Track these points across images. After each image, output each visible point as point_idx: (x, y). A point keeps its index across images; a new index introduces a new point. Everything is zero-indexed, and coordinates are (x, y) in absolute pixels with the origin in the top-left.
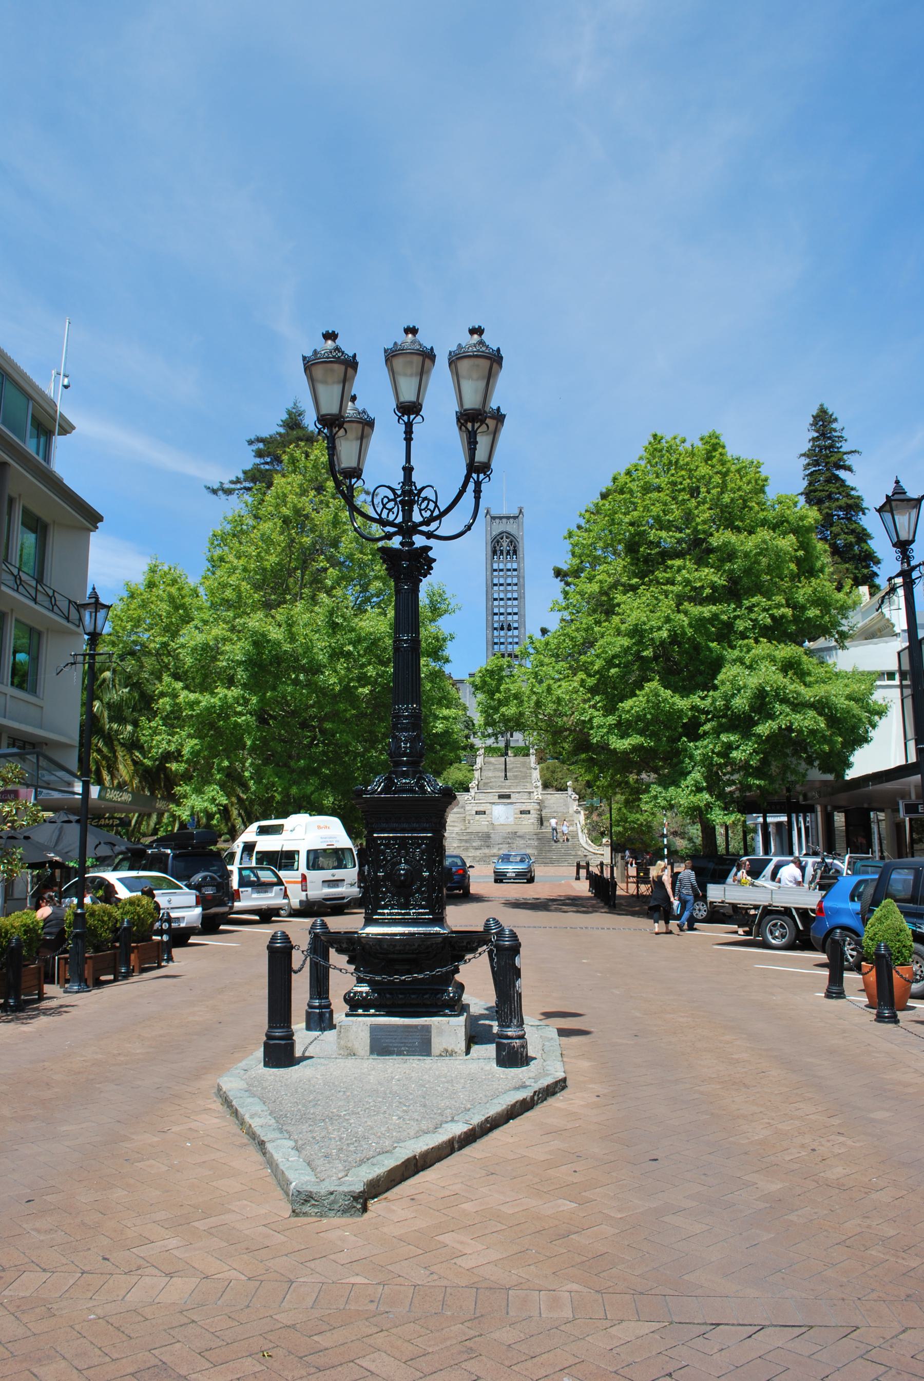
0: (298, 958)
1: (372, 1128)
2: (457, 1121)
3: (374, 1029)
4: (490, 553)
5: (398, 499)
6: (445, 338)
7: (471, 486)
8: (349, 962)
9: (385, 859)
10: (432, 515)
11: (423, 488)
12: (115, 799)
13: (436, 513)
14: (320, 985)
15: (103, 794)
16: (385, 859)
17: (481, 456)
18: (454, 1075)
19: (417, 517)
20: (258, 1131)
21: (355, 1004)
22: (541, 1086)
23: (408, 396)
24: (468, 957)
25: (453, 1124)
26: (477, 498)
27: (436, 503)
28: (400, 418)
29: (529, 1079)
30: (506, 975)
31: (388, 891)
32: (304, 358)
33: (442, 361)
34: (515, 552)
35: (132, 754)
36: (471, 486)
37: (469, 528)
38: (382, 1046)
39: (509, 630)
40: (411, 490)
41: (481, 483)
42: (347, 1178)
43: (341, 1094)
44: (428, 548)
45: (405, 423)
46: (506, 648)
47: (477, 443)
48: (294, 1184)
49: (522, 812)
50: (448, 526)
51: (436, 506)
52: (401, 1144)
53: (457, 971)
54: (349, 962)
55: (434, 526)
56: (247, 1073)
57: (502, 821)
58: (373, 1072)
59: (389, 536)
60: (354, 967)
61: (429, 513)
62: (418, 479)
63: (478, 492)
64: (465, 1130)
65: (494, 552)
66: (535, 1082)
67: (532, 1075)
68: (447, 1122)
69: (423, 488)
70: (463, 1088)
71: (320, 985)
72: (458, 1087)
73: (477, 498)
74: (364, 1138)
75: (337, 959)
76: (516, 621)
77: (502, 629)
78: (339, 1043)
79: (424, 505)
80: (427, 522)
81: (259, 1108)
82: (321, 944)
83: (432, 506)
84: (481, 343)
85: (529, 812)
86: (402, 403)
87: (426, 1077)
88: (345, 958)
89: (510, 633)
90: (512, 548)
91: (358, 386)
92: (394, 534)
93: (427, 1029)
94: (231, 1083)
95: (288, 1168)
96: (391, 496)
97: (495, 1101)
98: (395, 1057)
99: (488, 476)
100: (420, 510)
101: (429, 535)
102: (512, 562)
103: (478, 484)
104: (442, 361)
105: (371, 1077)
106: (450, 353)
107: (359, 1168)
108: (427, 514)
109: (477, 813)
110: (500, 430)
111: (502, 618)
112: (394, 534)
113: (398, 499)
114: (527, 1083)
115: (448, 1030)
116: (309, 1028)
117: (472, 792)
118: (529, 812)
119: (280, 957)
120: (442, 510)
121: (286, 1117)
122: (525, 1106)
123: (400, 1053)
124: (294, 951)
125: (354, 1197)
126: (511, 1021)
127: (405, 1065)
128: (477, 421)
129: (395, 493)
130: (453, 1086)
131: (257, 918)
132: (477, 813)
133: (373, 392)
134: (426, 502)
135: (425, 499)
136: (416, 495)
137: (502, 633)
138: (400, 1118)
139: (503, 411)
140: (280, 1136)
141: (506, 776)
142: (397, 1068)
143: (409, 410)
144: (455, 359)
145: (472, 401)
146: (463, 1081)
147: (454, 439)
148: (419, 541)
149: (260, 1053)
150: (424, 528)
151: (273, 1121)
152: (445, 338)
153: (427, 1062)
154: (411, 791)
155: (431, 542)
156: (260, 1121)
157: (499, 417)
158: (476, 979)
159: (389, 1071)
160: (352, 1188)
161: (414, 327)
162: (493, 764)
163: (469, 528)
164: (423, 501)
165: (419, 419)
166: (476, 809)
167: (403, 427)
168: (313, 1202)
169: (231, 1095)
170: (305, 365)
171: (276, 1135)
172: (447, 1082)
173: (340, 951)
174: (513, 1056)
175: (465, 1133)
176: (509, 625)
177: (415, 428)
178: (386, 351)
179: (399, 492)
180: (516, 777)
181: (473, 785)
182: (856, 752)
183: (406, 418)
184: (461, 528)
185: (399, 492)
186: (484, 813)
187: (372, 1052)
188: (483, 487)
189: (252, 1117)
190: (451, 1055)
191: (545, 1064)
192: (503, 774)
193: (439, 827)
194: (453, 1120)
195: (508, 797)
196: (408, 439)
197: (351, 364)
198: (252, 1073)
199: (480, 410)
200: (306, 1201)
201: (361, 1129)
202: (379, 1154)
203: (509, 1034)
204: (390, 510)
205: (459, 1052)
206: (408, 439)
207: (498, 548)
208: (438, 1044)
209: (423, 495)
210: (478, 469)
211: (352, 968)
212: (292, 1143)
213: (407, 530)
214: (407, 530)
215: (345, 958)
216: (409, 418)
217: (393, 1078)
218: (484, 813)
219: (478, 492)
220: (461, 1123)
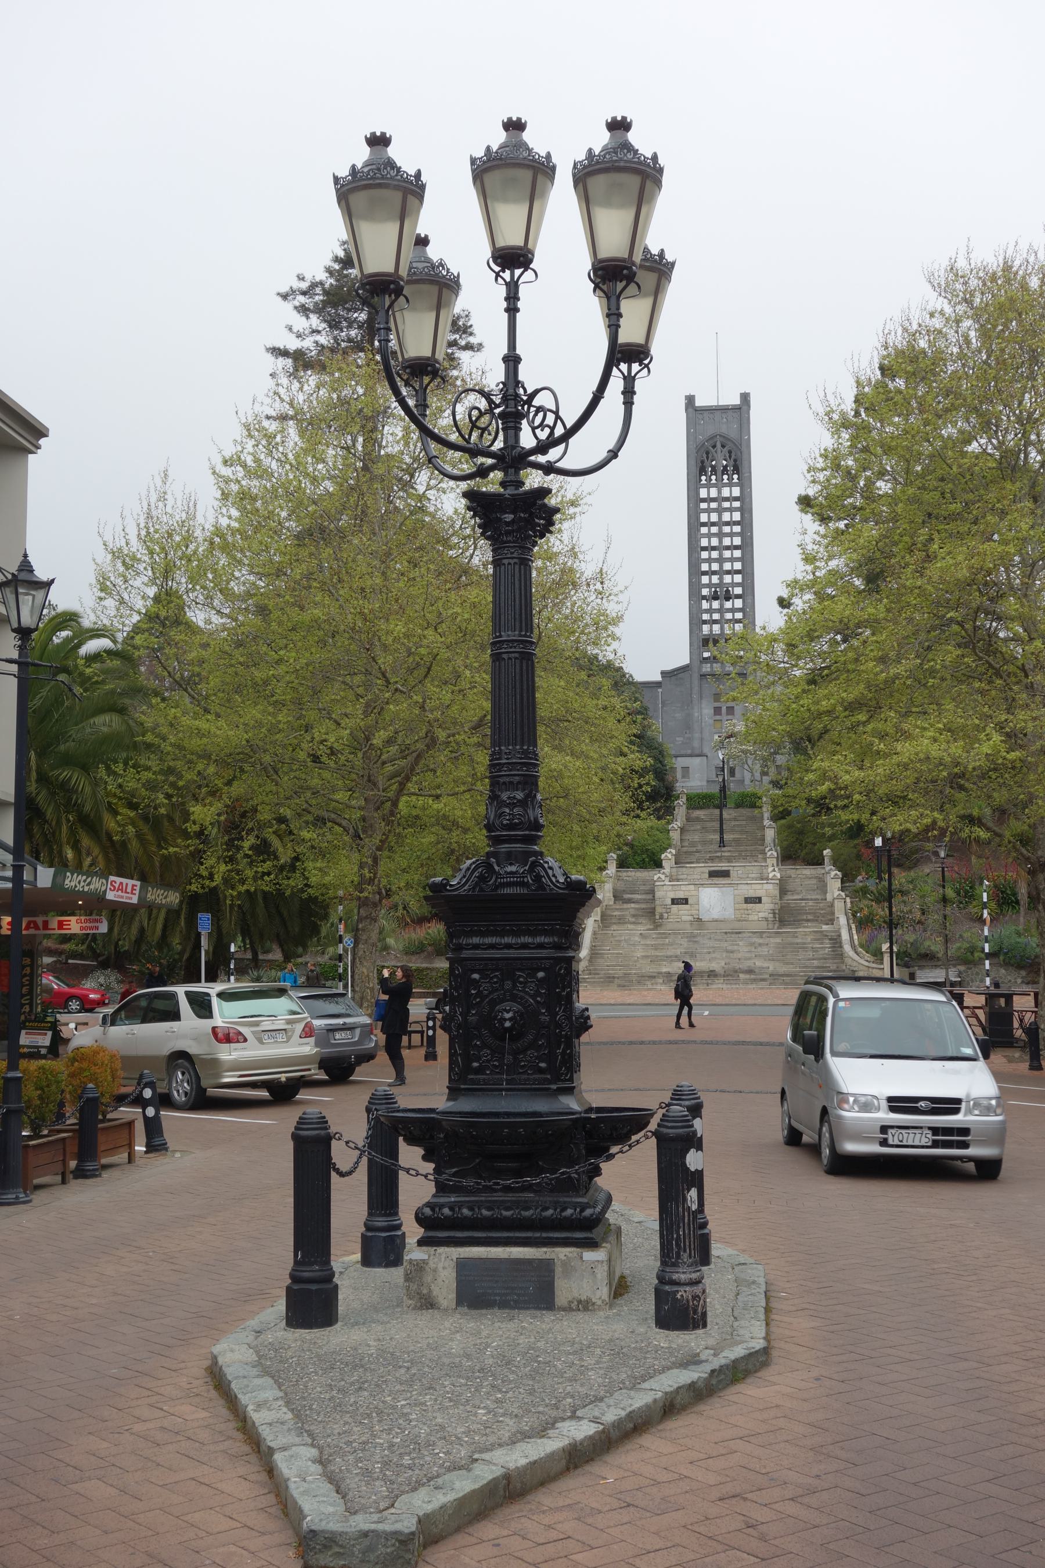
0: (341, 1155)
1: (442, 1428)
2: (580, 1418)
3: (462, 1266)
4: (695, 471)
5: (497, 411)
6: (566, 139)
7: (616, 384)
8: (425, 1158)
9: (479, 994)
10: (552, 433)
11: (537, 392)
12: (79, 888)
13: (559, 431)
14: (383, 1194)
15: (59, 880)
16: (479, 994)
17: (630, 333)
18: (591, 1337)
19: (527, 440)
20: (265, 1432)
21: (438, 1227)
22: (723, 1362)
23: (513, 238)
24: (614, 1150)
25: (573, 1423)
26: (628, 404)
27: (556, 413)
28: (497, 275)
29: (709, 1348)
30: (676, 1181)
31: (485, 1045)
32: (336, 180)
33: (564, 178)
34: (737, 469)
35: (1037, 420)
36: (616, 384)
37: (614, 454)
38: (477, 1293)
39: (727, 599)
40: (517, 395)
41: (634, 378)
42: (393, 1510)
43: (403, 1371)
44: (544, 492)
45: (507, 284)
46: (722, 628)
47: (620, 315)
48: (309, 1518)
49: (748, 900)
50: (581, 451)
51: (558, 417)
52: (486, 1456)
53: (597, 1171)
54: (425, 1158)
55: (553, 454)
56: (250, 1340)
57: (715, 914)
58: (458, 1336)
59: (482, 472)
60: (433, 1166)
61: (547, 431)
62: (529, 377)
63: (629, 393)
64: (591, 1433)
65: (702, 470)
66: (715, 1355)
67: (711, 1342)
68: (563, 1419)
69: (537, 392)
70: (598, 1363)
71: (383, 1194)
72: (589, 1361)
73: (628, 404)
74: (429, 1444)
75: (410, 1155)
76: (738, 585)
77: (715, 597)
78: (408, 1288)
79: (538, 421)
80: (542, 448)
81: (270, 1393)
82: (388, 1130)
83: (550, 419)
84: (627, 147)
85: (758, 900)
86: (503, 249)
87: (541, 1344)
88: (419, 1151)
89: (728, 605)
90: (732, 462)
91: (428, 220)
92: (492, 468)
93: (546, 1267)
94: (234, 1353)
95: (306, 1492)
96: (483, 404)
97: (646, 1385)
98: (496, 1310)
99: (647, 366)
100: (534, 429)
101: (549, 469)
102: (730, 485)
103: (629, 382)
104: (564, 178)
105: (454, 1344)
106: (575, 164)
107: (415, 1494)
108: (543, 435)
109: (674, 901)
110: (665, 290)
111: (715, 579)
112: (492, 468)
113: (497, 411)
114: (703, 1357)
115: (581, 1271)
116: (367, 1261)
117: (667, 870)
118: (758, 900)
119: (312, 1154)
120: (569, 424)
121: (311, 1409)
122: (699, 1394)
123: (504, 1305)
124: (334, 1142)
125: (401, 1542)
126: (678, 1256)
127: (511, 1325)
128: (623, 277)
129: (490, 402)
130: (581, 1359)
131: (264, 1094)
132: (674, 901)
133: (454, 229)
134: (541, 415)
135: (539, 409)
136: (525, 402)
137: (716, 605)
138: (489, 1412)
139: (669, 257)
140: (297, 1440)
141: (722, 838)
142: (500, 1331)
143: (512, 259)
144: (586, 174)
145: (613, 245)
146: (598, 1351)
147: (591, 306)
148: (533, 479)
149: (281, 1306)
150: (541, 459)
151: (290, 1415)
152: (566, 139)
153: (549, 1317)
154: (523, 884)
155: (553, 481)
156: (268, 1415)
157: (660, 269)
158: (628, 1183)
159: (484, 1333)
160: (398, 1527)
161: (519, 119)
162: (703, 820)
163: (614, 454)
164: (536, 415)
165: (529, 275)
166: (672, 895)
167: (502, 291)
168: (337, 1549)
169: (230, 1372)
170: (337, 191)
171: (292, 1438)
172: (575, 1353)
173: (411, 1141)
174: (678, 1313)
175: (591, 1437)
176: (728, 591)
177: (523, 291)
178: (473, 161)
179: (497, 400)
180: (737, 841)
181: (668, 857)
182: (365, 1126)
183: (507, 275)
184: (603, 455)
185: (497, 400)
186: (685, 901)
187: (461, 1300)
188: (638, 385)
189: (259, 1406)
190: (586, 1309)
191: (736, 1324)
192: (717, 837)
193: (571, 938)
194: (573, 1417)
195: (725, 874)
196: (512, 310)
197: (412, 190)
198: (269, 1337)
199: (623, 260)
200: (325, 1546)
201: (424, 1430)
202: (449, 1470)
203: (675, 1277)
204: (484, 430)
205: (599, 1302)
206: (512, 310)
207: (707, 463)
208: (565, 1290)
209: (536, 402)
210: (627, 355)
211: (429, 1167)
212: (314, 1452)
213: (514, 460)
214: (514, 460)
215: (419, 1151)
216: (512, 275)
217: (488, 1345)
218: (685, 901)
219: (629, 393)
220: (586, 1421)
